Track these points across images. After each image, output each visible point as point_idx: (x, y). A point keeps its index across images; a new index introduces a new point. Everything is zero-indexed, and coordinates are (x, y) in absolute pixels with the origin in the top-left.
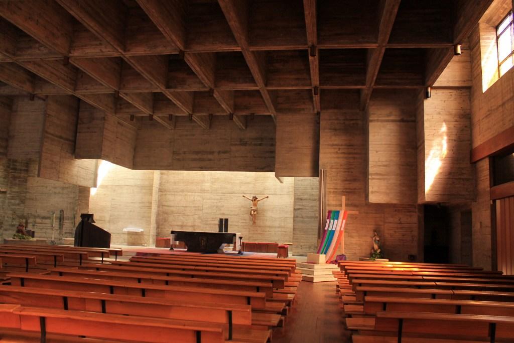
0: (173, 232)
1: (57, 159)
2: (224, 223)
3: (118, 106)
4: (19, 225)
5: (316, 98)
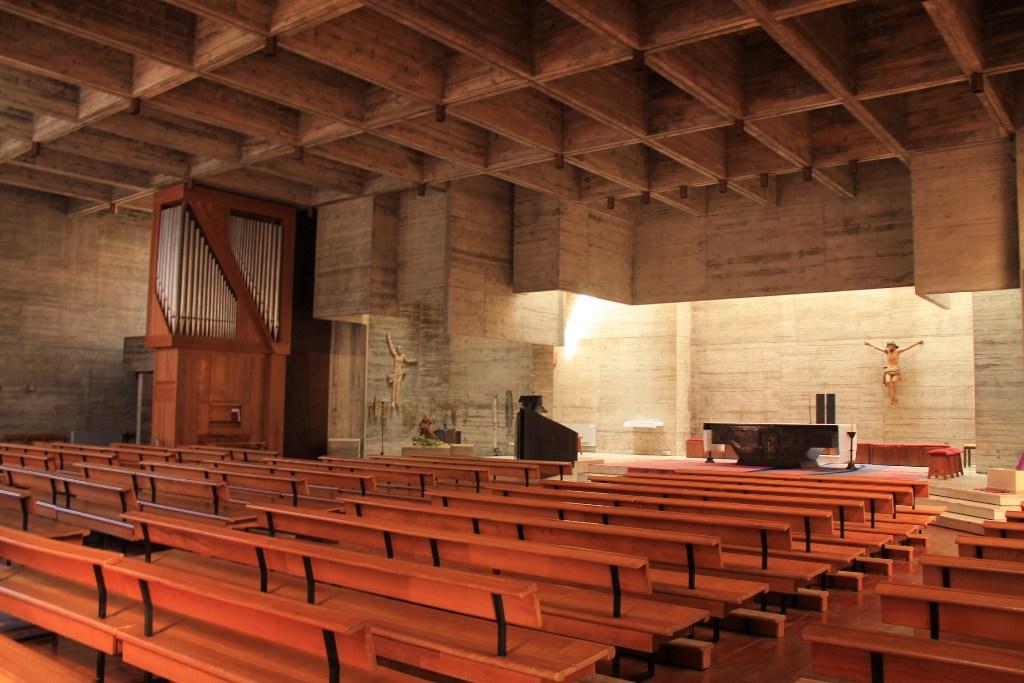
0: (707, 426)
1: (478, 296)
2: (826, 404)
3: (584, 184)
4: (423, 421)
5: (989, 98)
